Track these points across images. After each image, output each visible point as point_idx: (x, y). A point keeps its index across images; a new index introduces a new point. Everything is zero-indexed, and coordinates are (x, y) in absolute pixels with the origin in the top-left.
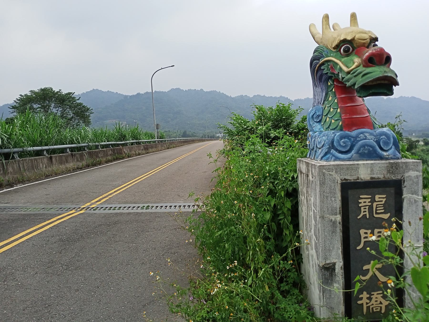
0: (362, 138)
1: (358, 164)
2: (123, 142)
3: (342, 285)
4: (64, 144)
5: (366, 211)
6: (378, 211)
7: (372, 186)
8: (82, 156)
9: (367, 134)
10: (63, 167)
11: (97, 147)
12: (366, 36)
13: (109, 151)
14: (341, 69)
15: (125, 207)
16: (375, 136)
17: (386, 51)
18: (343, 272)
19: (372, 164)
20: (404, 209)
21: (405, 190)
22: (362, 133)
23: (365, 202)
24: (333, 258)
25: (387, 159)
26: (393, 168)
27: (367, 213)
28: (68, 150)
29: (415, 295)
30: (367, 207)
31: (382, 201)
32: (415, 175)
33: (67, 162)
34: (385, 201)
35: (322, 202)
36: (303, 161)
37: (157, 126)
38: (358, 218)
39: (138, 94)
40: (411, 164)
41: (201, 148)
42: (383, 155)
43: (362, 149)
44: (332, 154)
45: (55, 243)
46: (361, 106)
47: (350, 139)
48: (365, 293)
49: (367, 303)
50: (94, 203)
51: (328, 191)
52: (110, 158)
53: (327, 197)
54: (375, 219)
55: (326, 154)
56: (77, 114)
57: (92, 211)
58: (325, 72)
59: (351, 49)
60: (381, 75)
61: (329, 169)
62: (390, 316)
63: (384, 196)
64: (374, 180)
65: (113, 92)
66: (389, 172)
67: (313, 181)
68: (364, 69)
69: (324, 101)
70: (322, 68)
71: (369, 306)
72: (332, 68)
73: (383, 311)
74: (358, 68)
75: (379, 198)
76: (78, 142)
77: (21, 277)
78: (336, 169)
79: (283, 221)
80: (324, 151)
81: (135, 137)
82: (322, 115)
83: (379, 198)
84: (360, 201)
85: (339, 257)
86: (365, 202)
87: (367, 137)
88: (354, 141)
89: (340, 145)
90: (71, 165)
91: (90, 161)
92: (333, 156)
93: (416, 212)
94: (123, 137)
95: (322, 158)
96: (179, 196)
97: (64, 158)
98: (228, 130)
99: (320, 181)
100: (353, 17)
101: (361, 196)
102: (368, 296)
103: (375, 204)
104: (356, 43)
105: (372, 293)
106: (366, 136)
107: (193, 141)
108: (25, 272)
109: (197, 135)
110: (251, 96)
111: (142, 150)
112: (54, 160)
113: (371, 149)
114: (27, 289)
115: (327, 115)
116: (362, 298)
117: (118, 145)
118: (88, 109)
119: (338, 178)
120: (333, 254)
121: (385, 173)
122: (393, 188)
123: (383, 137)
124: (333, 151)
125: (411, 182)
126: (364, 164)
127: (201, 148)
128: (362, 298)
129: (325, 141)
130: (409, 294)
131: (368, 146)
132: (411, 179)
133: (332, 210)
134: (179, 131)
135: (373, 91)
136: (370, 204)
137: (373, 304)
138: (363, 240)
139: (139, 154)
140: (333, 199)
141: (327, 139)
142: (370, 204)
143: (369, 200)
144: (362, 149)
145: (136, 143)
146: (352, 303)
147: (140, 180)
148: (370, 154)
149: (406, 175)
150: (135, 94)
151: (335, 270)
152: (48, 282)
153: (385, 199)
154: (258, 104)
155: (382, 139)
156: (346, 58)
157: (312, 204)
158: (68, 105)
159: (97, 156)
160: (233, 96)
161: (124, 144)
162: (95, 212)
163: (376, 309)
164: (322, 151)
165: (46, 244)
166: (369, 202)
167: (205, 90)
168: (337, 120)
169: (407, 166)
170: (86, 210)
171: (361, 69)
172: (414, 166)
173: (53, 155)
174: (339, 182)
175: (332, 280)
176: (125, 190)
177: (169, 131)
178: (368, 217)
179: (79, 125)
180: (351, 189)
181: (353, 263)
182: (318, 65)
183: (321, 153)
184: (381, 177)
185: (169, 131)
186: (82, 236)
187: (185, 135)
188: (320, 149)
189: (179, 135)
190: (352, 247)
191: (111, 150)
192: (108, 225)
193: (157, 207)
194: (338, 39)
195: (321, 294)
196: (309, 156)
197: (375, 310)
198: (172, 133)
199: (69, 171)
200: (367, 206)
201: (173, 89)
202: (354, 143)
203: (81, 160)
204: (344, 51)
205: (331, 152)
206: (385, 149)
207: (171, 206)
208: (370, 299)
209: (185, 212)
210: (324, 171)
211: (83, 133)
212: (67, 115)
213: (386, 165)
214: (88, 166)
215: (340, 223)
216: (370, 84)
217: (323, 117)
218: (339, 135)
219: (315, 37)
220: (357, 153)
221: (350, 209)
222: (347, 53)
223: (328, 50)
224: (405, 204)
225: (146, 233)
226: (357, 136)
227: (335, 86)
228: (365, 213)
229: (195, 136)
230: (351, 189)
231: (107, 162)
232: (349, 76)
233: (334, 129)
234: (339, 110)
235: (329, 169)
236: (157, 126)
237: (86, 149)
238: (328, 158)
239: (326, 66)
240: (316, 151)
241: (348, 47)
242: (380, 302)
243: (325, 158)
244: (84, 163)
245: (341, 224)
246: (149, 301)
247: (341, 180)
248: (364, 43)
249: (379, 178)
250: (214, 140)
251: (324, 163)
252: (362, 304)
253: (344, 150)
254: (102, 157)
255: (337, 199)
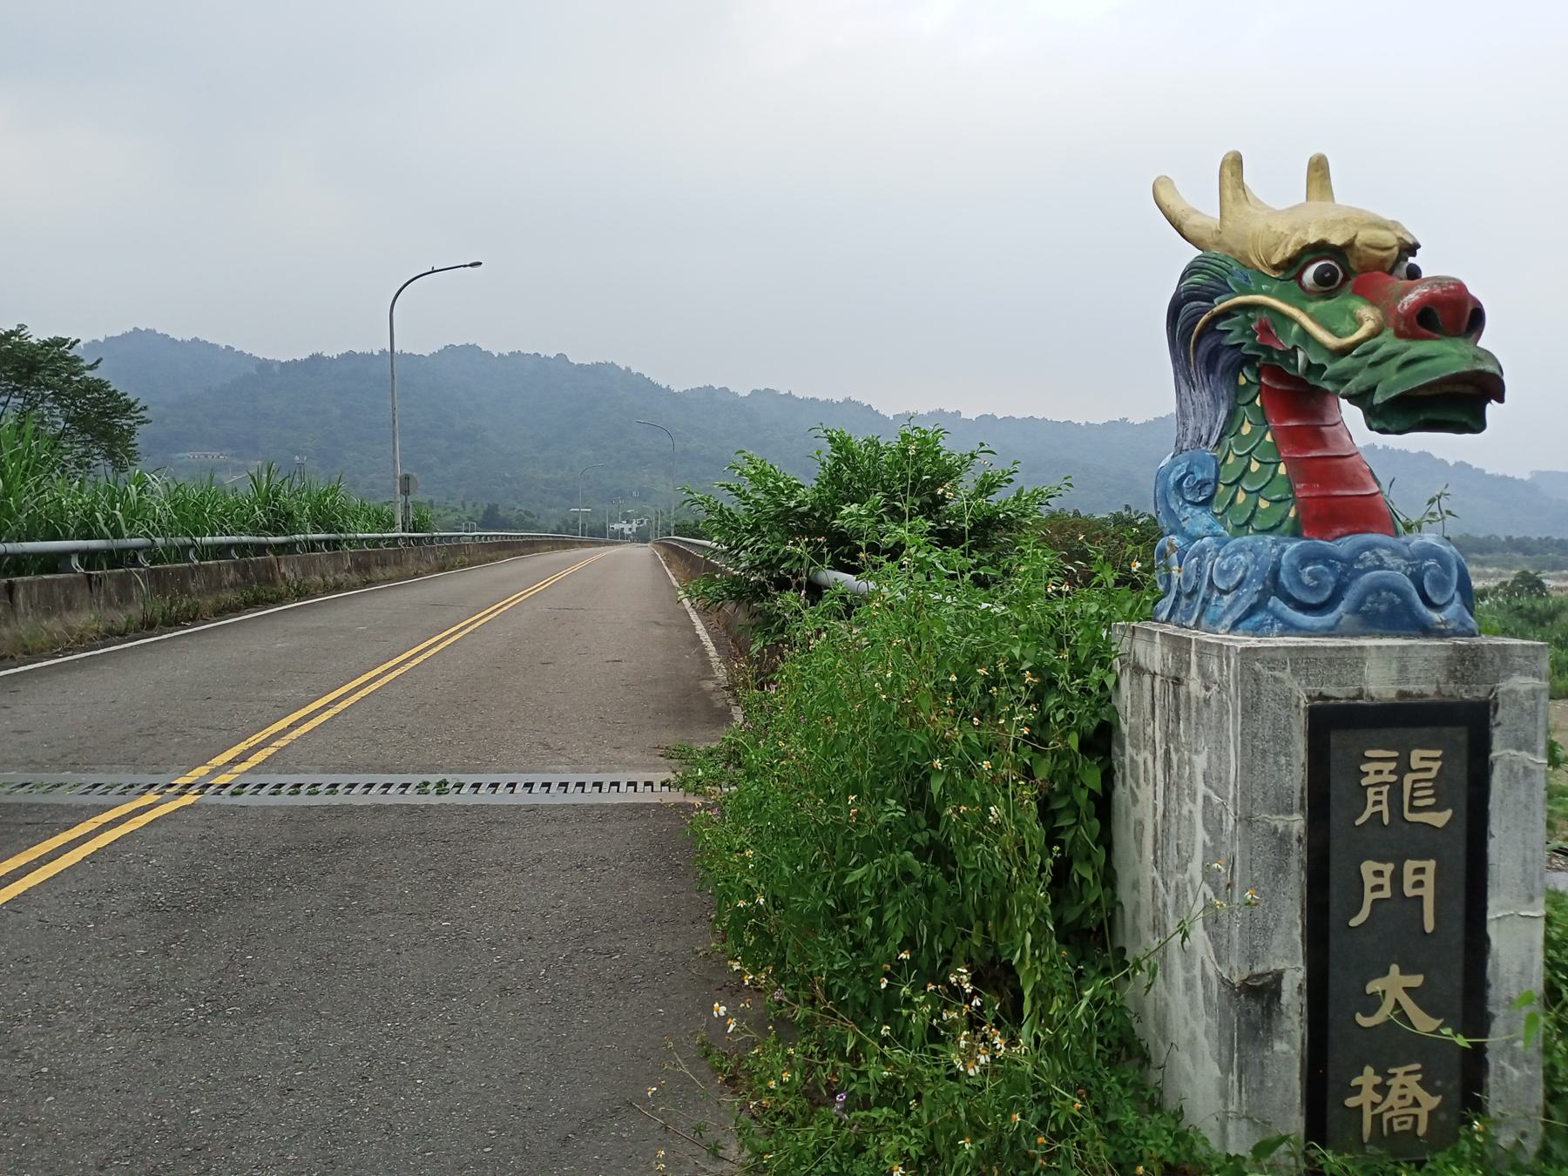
0: (1368, 563)
1: (1361, 648)
2: (281, 539)
3: (1299, 1046)
4: (56, 537)
5: (1380, 802)
6: (1417, 803)
7: (1403, 719)
8: (125, 584)
9: (1383, 553)
10: (54, 625)
11: (182, 553)
12: (1390, 238)
13: (228, 572)
14: (1305, 334)
15: (262, 786)
16: (1407, 559)
17: (1472, 291)
18: (1305, 1001)
19: (1403, 648)
20: (1492, 797)
21: (1497, 735)
22: (1369, 547)
23: (1379, 772)
24: (1276, 957)
25: (1441, 634)
26: (1466, 662)
27: (1384, 808)
28: (75, 561)
29: (1516, 1073)
30: (1385, 789)
31: (1429, 769)
32: (1529, 687)
33: (69, 607)
34: (1440, 770)
35: (1247, 768)
36: (1151, 633)
37: (406, 484)
38: (1358, 822)
39: (316, 359)
40: (1518, 652)
41: (570, 570)
42: (1431, 619)
43: (1370, 599)
44: (1271, 611)
45: (129, 915)
46: (1340, 461)
47: (1330, 566)
48: (1369, 1070)
49: (1374, 1105)
50: (226, 767)
51: (1268, 733)
52: (230, 596)
53: (1264, 751)
54: (1407, 827)
55: (1252, 611)
56: (81, 422)
57: (225, 799)
58: (1230, 340)
59: (1341, 275)
60: (1464, 368)
61: (1273, 660)
62: (1463, 1142)
63: (1438, 753)
64: (1408, 700)
65: (215, 346)
66: (1452, 675)
67: (1207, 701)
68: (1402, 343)
69: (1221, 436)
70: (1220, 327)
71: (1381, 1114)
72: (1265, 329)
73: (1422, 1129)
74: (1379, 339)
75: (1422, 759)
76: (111, 530)
77: (41, 1044)
78: (1294, 662)
79: (1071, 833)
80: (1243, 601)
81: (323, 519)
82: (1217, 480)
83: (1422, 759)
84: (1364, 768)
85: (1294, 951)
86: (1379, 772)
87: (1383, 560)
88: (1343, 573)
89: (1300, 583)
90: (84, 619)
91: (157, 606)
92: (1278, 617)
93: (1527, 807)
94: (282, 520)
95: (1235, 626)
96: (547, 746)
97: (56, 590)
98: (721, 511)
99: (1244, 699)
100: (1319, 169)
101: (1368, 754)
102: (1378, 1080)
103: (1408, 779)
104: (1359, 259)
105: (1391, 1071)
106: (1380, 559)
107: (532, 546)
108: (49, 1024)
109: (541, 522)
110: (744, 392)
111: (349, 571)
112: (20, 596)
113: (1398, 600)
114: (82, 1089)
115: (1237, 482)
116: (1360, 1087)
117: (261, 549)
118: (130, 406)
119: (1300, 692)
120: (1275, 943)
121: (1442, 679)
122: (1463, 727)
123: (1431, 562)
124: (1275, 602)
125: (1515, 711)
126: (1379, 647)
127: (570, 570)
128: (1360, 1087)
129: (1247, 568)
130: (1503, 1073)
131: (1389, 589)
132: (1515, 701)
133: (1277, 797)
134: (469, 505)
135: (1430, 415)
136: (1393, 778)
137: (1391, 1108)
138: (1369, 896)
139: (338, 588)
140: (1283, 760)
141: (1255, 562)
142: (1393, 778)
143: (1393, 765)
144: (1370, 599)
145: (327, 542)
146: (1330, 1104)
147: (373, 687)
148: (1394, 615)
149: (1504, 686)
150: (302, 355)
151: (1279, 996)
152: (159, 1063)
153: (1439, 763)
154: (836, 426)
155: (1428, 568)
156: (1321, 304)
157: (1200, 777)
158: (48, 387)
159: (184, 590)
160: (676, 389)
161: (283, 545)
162: (238, 800)
163: (1401, 1124)
164: (1237, 599)
165: (94, 919)
166: (1391, 772)
167: (574, 359)
168: (1279, 501)
169: (1504, 659)
170: (201, 793)
171: (1388, 342)
172: (1527, 658)
173: (18, 579)
174: (1302, 704)
175: (1269, 1030)
176: (331, 720)
177: (431, 502)
178: (1386, 821)
179: (88, 464)
180: (1336, 727)
181: (1335, 971)
182: (1205, 317)
183: (1231, 607)
184: (1430, 690)
185: (431, 502)
186: (227, 893)
187: (490, 519)
188: (1226, 592)
189: (470, 519)
190: (1334, 921)
191: (236, 565)
192: (304, 854)
193: (370, 786)
194: (1294, 239)
195: (1233, 1078)
196: (1170, 615)
197: (1397, 1128)
198: (441, 512)
199: (82, 642)
200: (1385, 783)
201: (451, 349)
202: (1345, 580)
203: (121, 600)
204: (1318, 277)
205: (1270, 604)
206: (1436, 600)
207: (495, 785)
208: (1383, 1089)
209: (592, 806)
210: (1258, 666)
211: (134, 497)
212: (43, 423)
213: (1444, 654)
214: (148, 626)
215: (1299, 840)
216: (1424, 393)
217: (1221, 487)
218: (1296, 551)
219: (1189, 223)
220: (1355, 610)
221: (1333, 793)
222: (1328, 285)
223: (1248, 272)
224: (1497, 781)
225: (477, 882)
226: (1354, 558)
227: (1265, 391)
228: (1378, 808)
229: (529, 527)
230: (1336, 727)
231: (220, 613)
232: (1345, 362)
233: (1270, 531)
234: (1282, 469)
235: (1272, 658)
236: (406, 484)
237: (141, 558)
238: (1261, 625)
239: (1236, 323)
240: (1206, 601)
241: (1340, 267)
242: (1415, 1099)
243: (1246, 623)
244: (135, 612)
245: (1305, 841)
246: (575, 1124)
247: (1309, 697)
248: (1384, 260)
249: (1421, 695)
250: (607, 544)
251: (1253, 642)
252: (1360, 1108)
253: (1313, 600)
254: (200, 593)
255: (1294, 762)
